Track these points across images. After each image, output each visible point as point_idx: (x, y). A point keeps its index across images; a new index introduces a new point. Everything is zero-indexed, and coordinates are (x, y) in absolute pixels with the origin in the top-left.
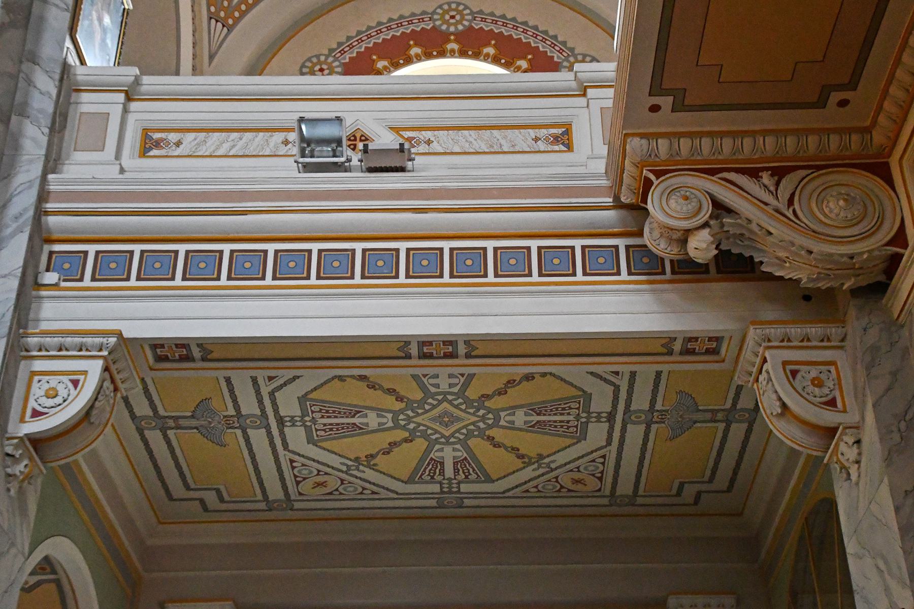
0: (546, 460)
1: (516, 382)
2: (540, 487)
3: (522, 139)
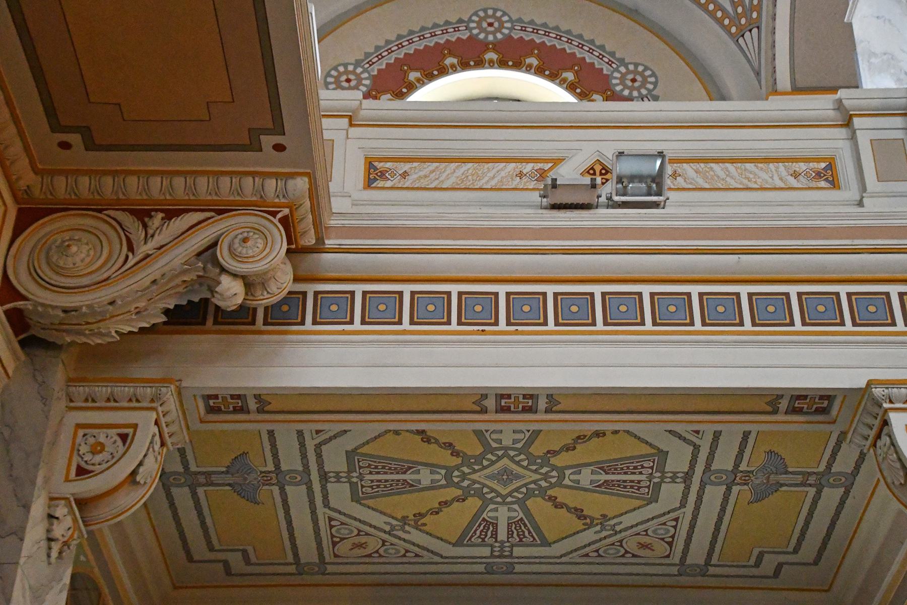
0: (612, 522)
1: (587, 438)
2: (601, 552)
3: (778, 174)
